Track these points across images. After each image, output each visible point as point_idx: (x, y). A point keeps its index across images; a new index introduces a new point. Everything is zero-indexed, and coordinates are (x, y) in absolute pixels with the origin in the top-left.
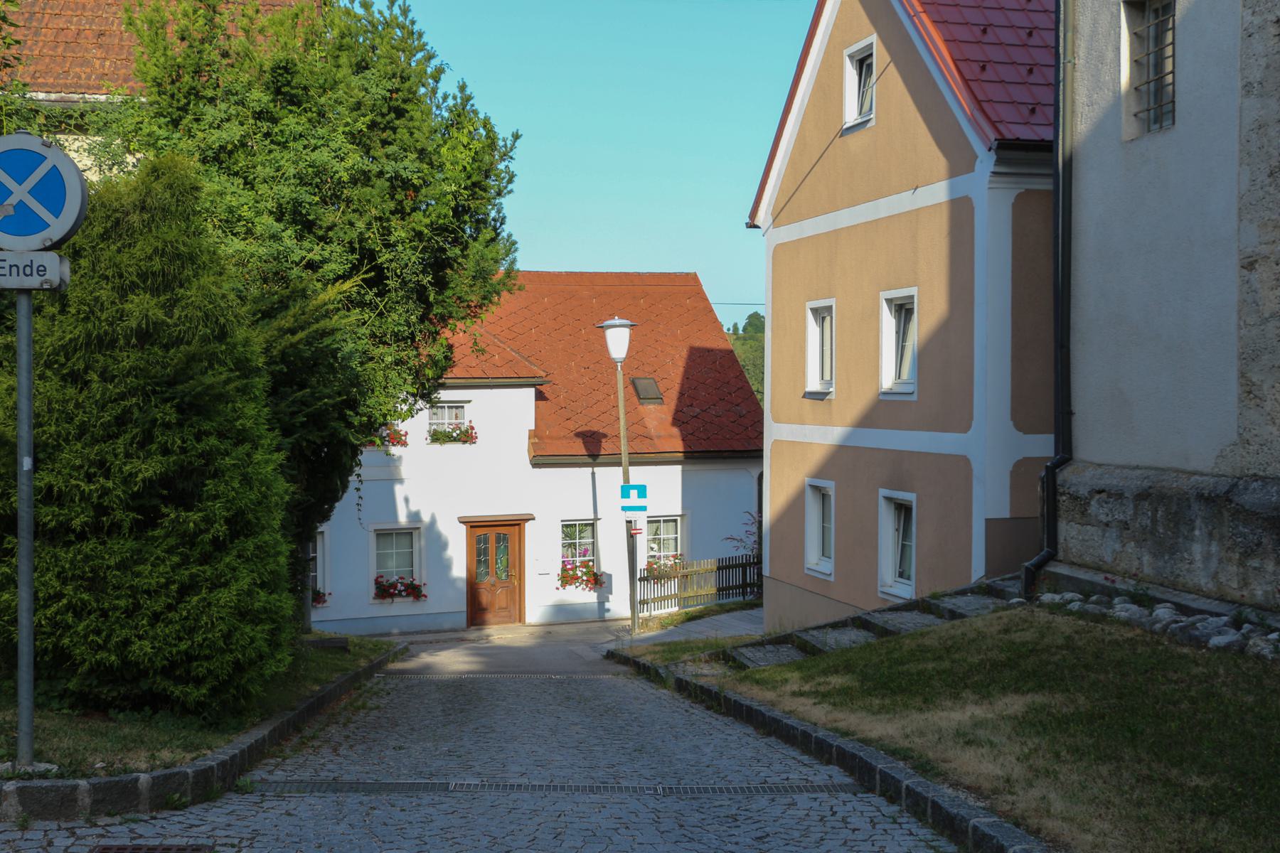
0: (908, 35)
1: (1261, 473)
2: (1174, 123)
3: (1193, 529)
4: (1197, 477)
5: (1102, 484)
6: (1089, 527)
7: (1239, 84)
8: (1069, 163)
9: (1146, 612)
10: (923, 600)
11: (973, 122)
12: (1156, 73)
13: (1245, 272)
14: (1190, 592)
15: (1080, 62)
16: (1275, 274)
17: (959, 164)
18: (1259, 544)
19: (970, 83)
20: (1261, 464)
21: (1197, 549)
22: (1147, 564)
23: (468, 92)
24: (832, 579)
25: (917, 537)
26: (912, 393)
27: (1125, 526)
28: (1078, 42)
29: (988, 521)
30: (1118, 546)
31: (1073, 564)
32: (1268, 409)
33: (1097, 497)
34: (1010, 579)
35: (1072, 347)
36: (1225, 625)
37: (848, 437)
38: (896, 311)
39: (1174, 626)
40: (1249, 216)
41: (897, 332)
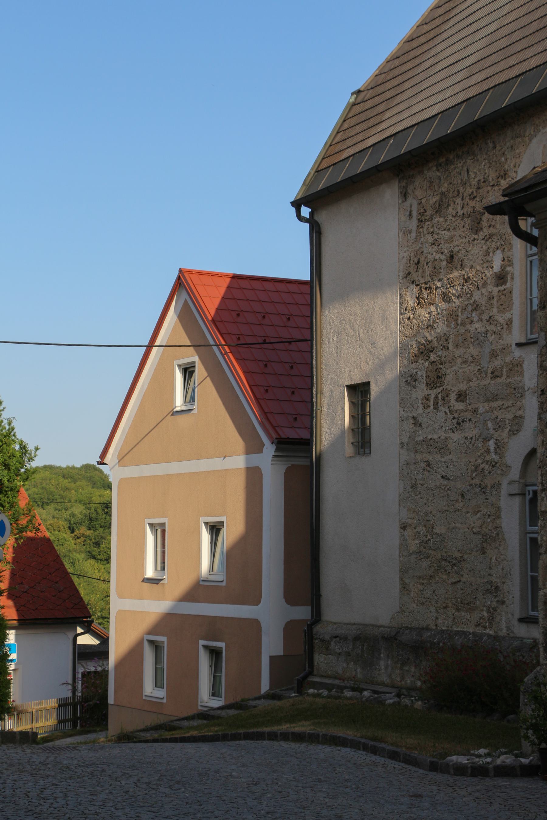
0: (220, 362)
1: (410, 626)
2: (370, 453)
3: (380, 654)
4: (382, 629)
6: (330, 656)
7: (399, 442)
8: (319, 458)
9: (359, 693)
10: (237, 703)
11: (262, 424)
12: (362, 411)
13: (402, 531)
14: (379, 685)
15: (324, 410)
16: (414, 533)
18: (408, 659)
19: (259, 400)
20: (409, 622)
21: (382, 663)
22: (359, 673)
23: (12, 425)
24: (164, 701)
25: (226, 669)
26: (223, 581)
27: (348, 654)
28: (323, 399)
29: (271, 658)
30: (345, 665)
31: (322, 676)
32: (412, 596)
33: (334, 640)
34: (285, 690)
35: (320, 560)
36: (394, 696)
38: (210, 529)
39: (371, 698)
40: (403, 505)
41: (211, 543)
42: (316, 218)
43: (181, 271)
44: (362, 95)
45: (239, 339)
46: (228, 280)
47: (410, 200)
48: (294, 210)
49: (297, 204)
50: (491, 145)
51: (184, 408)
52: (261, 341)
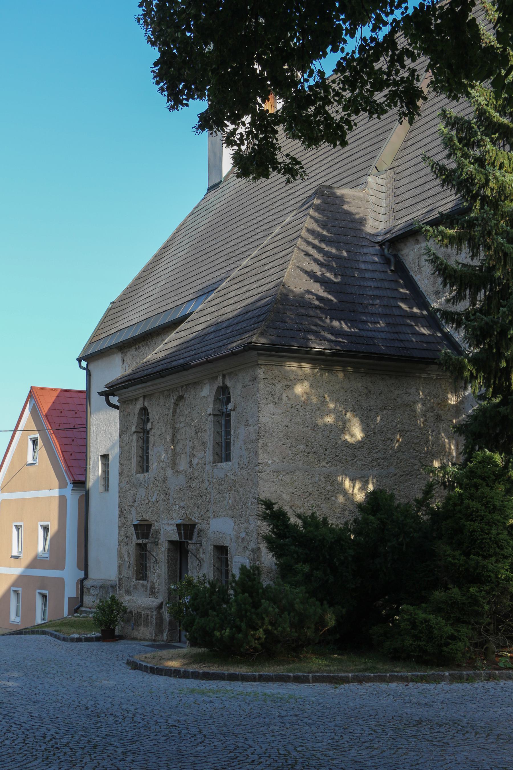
5: (93, 584)
17: (62, 486)
24: (20, 624)
37: (24, 572)
41: (44, 536)
42: (89, 368)
43: (31, 387)
44: (115, 304)
45: (59, 426)
46: (58, 392)
47: (125, 364)
48: (77, 363)
49: (79, 360)
50: (154, 342)
51: (32, 462)
52: (72, 426)
